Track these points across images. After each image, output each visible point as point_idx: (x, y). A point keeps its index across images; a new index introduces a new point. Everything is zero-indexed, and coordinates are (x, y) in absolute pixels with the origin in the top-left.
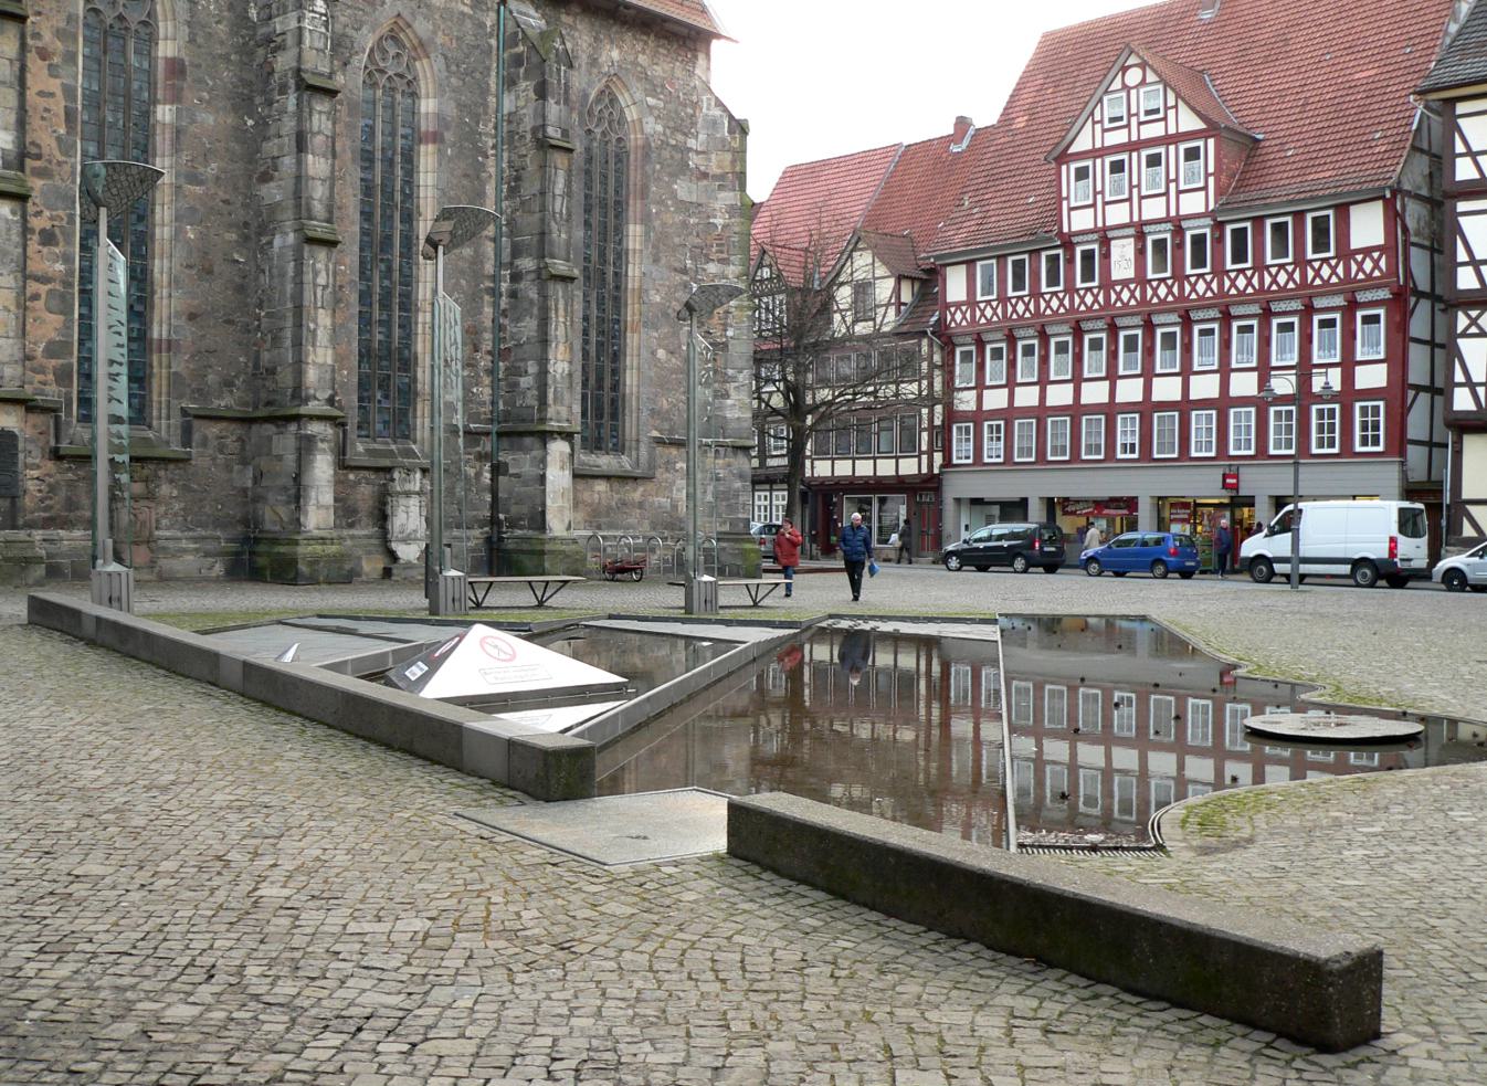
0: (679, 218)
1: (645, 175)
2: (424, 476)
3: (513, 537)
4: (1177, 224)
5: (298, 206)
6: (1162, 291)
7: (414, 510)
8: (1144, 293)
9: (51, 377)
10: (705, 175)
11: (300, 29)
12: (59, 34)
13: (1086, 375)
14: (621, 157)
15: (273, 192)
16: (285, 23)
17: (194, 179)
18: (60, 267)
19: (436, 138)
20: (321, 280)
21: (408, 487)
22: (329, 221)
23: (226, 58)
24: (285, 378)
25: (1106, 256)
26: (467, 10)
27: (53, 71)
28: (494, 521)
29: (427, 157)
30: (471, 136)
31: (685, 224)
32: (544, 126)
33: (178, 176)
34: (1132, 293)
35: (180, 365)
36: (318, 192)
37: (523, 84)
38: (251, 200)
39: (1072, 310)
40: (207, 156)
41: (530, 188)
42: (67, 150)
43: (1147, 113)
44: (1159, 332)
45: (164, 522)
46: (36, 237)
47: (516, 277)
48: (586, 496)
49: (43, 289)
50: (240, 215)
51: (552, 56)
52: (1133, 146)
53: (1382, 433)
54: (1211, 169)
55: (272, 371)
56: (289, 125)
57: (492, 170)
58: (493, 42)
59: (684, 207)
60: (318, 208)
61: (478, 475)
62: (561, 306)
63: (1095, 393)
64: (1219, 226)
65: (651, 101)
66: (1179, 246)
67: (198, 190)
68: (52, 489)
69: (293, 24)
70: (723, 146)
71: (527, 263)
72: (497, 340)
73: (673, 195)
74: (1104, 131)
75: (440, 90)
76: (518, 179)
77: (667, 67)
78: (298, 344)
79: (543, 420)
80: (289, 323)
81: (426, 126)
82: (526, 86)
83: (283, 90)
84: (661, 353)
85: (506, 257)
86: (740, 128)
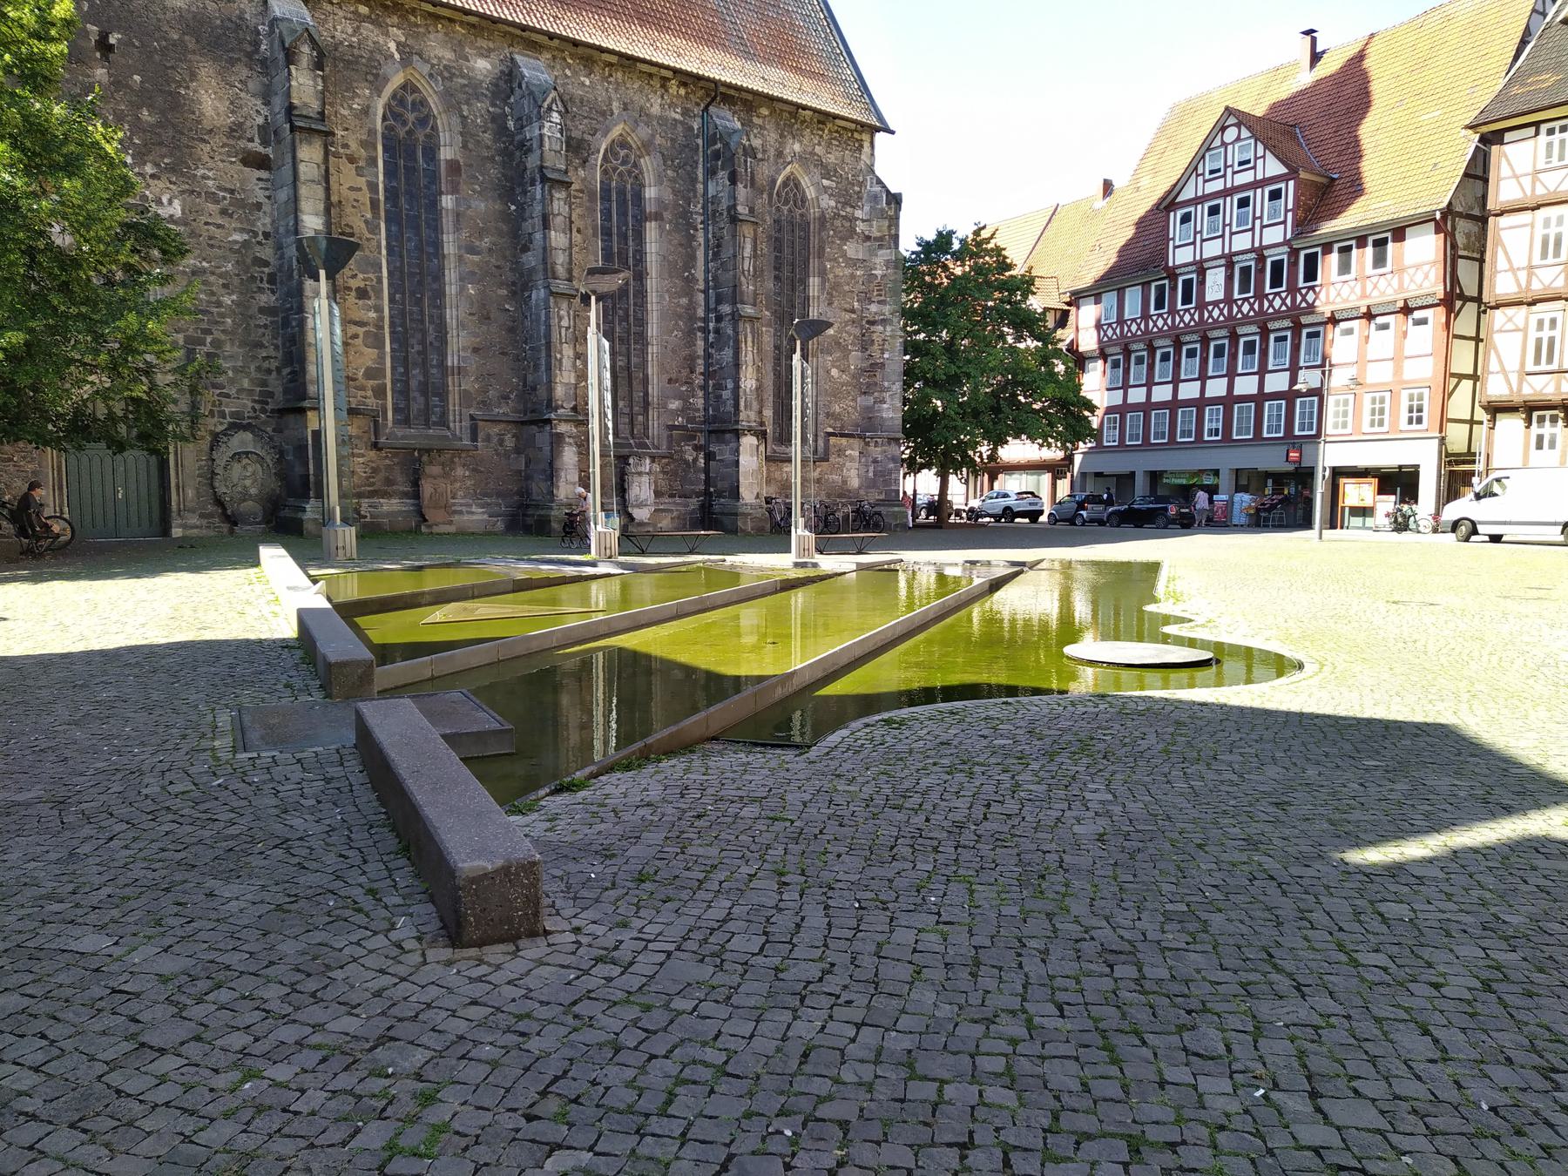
0: (848, 271)
1: (822, 241)
2: (653, 461)
3: (719, 504)
4: (1260, 253)
5: (545, 270)
6: (1246, 308)
7: (645, 486)
8: (1230, 310)
9: (370, 393)
10: (868, 238)
11: (541, 136)
12: (363, 144)
13: (1183, 377)
14: (805, 226)
15: (531, 259)
16: (531, 132)
17: (472, 250)
18: (372, 315)
19: (658, 217)
20: (565, 323)
21: (640, 469)
22: (570, 280)
23: (492, 159)
24: (542, 392)
25: (1202, 283)
26: (678, 117)
27: (359, 172)
28: (706, 493)
29: (651, 230)
30: (685, 215)
31: (853, 276)
32: (734, 206)
33: (459, 248)
34: (1221, 311)
35: (470, 384)
36: (560, 259)
37: (721, 174)
38: (517, 267)
39: (1174, 327)
40: (481, 233)
41: (726, 253)
42: (374, 229)
43: (1241, 164)
44: (1242, 340)
45: (460, 493)
46: (353, 294)
47: (719, 319)
48: (777, 474)
49: (361, 331)
50: (509, 276)
51: (740, 151)
52: (1226, 193)
53: (1425, 414)
54: (1290, 206)
55: (534, 389)
56: (538, 208)
57: (701, 240)
58: (700, 141)
59: (853, 263)
60: (561, 271)
61: (696, 460)
62: (749, 339)
63: (1189, 391)
64: (1294, 253)
65: (825, 182)
66: (1261, 271)
67: (476, 258)
68: (375, 470)
69: (537, 132)
70: (882, 215)
71: (726, 309)
72: (707, 365)
73: (844, 255)
74: (1205, 181)
75: (659, 181)
76: (719, 246)
77: (839, 155)
78: (549, 368)
79: (737, 422)
80: (543, 354)
81: (650, 208)
82: (723, 175)
83: (533, 184)
84: (834, 372)
85: (712, 306)
86: (895, 200)
